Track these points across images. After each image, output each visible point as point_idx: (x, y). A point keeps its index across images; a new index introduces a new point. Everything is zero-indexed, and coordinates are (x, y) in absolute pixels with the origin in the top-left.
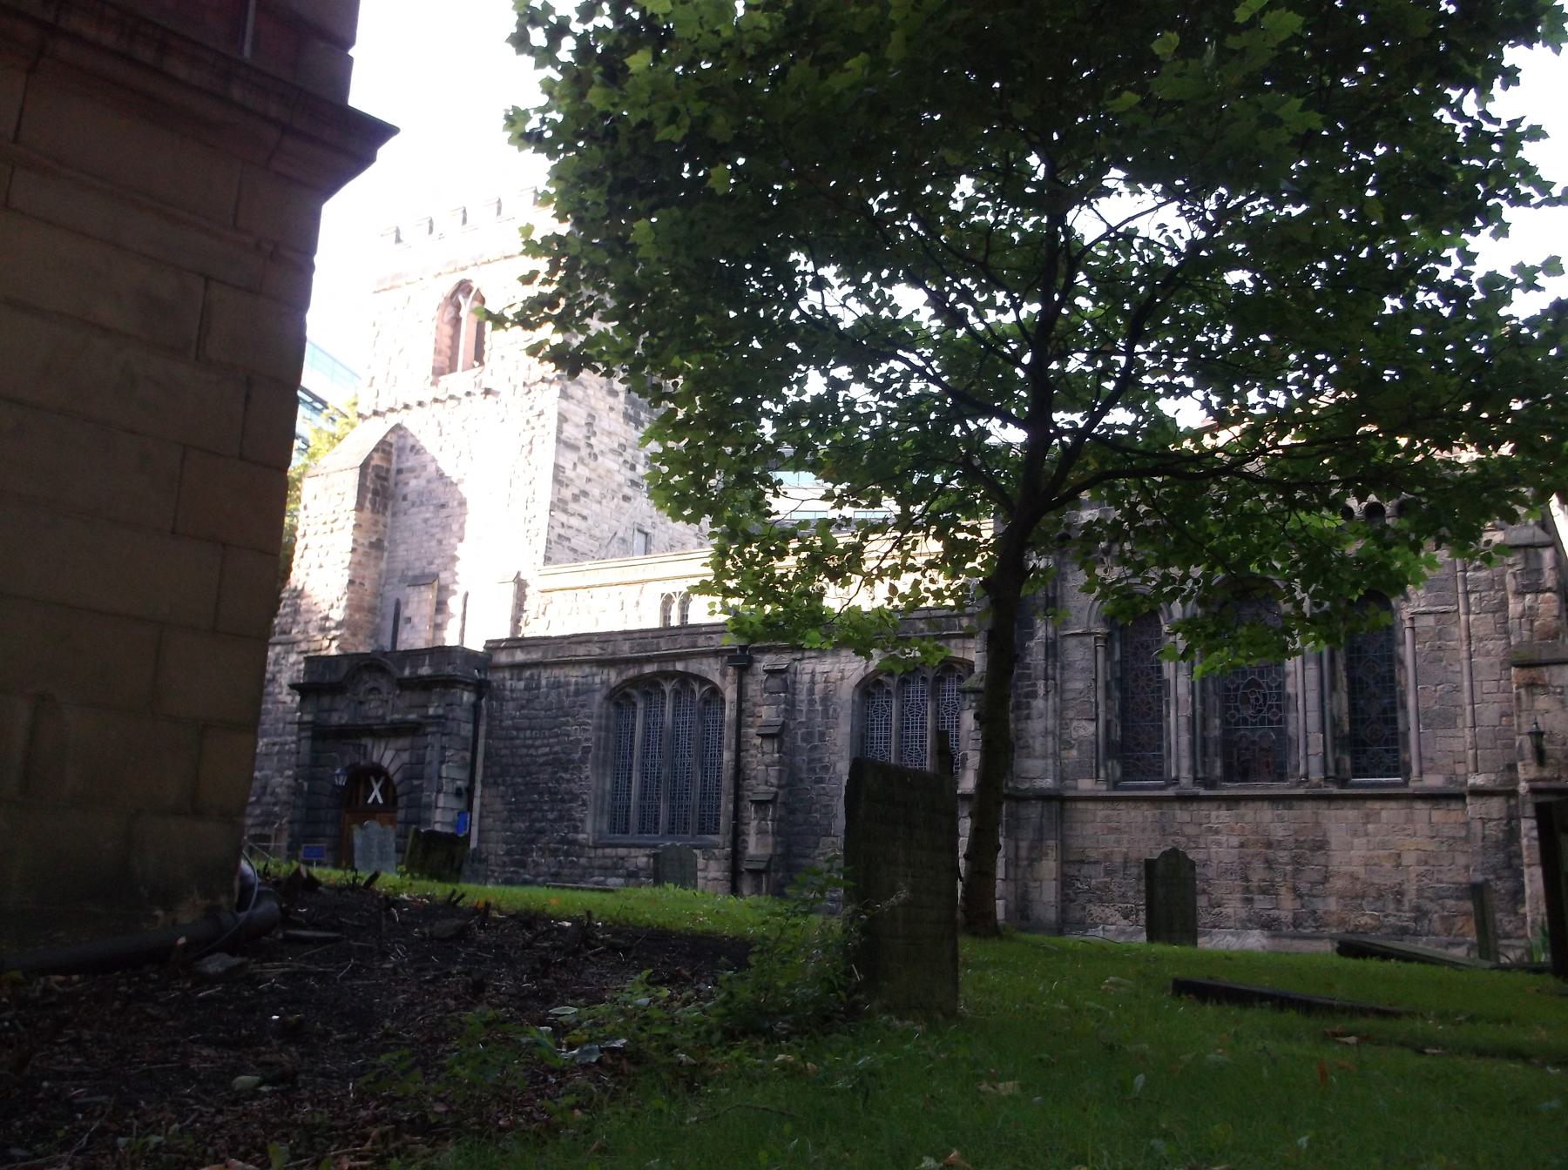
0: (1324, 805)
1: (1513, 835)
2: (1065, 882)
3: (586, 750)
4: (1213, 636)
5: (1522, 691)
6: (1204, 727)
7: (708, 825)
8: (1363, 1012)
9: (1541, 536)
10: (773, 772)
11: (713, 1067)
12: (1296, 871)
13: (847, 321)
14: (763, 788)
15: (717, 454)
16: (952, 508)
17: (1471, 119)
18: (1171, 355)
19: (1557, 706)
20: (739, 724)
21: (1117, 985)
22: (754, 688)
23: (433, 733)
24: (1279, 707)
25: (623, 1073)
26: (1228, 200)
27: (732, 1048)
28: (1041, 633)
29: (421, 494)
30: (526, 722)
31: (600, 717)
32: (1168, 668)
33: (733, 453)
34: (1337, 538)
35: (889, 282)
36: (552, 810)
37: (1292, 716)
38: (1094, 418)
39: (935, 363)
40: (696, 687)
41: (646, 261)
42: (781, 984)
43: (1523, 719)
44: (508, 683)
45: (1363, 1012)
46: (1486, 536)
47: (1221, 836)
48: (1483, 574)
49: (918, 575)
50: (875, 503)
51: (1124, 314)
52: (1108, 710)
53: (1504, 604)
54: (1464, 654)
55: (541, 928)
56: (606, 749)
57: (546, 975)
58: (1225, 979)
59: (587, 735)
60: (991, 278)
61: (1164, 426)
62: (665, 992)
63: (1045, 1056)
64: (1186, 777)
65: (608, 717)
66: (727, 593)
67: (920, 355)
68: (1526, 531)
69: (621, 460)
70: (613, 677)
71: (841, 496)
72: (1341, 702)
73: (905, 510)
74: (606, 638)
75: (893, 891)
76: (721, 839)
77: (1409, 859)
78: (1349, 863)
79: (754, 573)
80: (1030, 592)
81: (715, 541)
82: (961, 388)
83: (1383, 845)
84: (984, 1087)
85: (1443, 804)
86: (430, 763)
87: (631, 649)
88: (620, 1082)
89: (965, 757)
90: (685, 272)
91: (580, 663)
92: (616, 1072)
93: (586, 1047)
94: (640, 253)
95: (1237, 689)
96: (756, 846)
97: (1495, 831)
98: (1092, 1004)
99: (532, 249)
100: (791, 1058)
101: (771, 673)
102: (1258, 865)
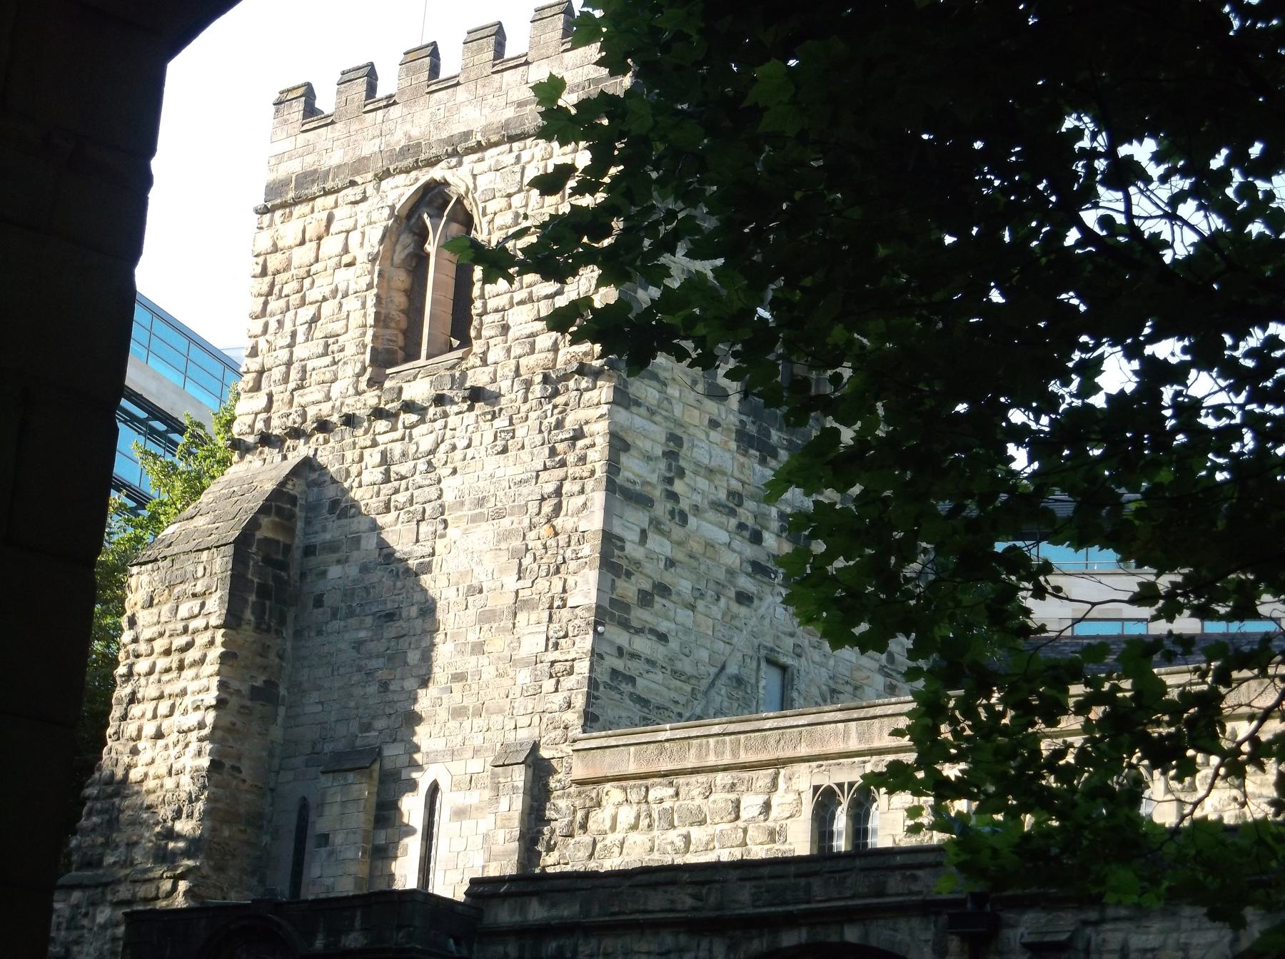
29: (348, 594)
69: (733, 522)
71: (1171, 595)
79: (998, 750)
81: (920, 684)
91: (656, 926)
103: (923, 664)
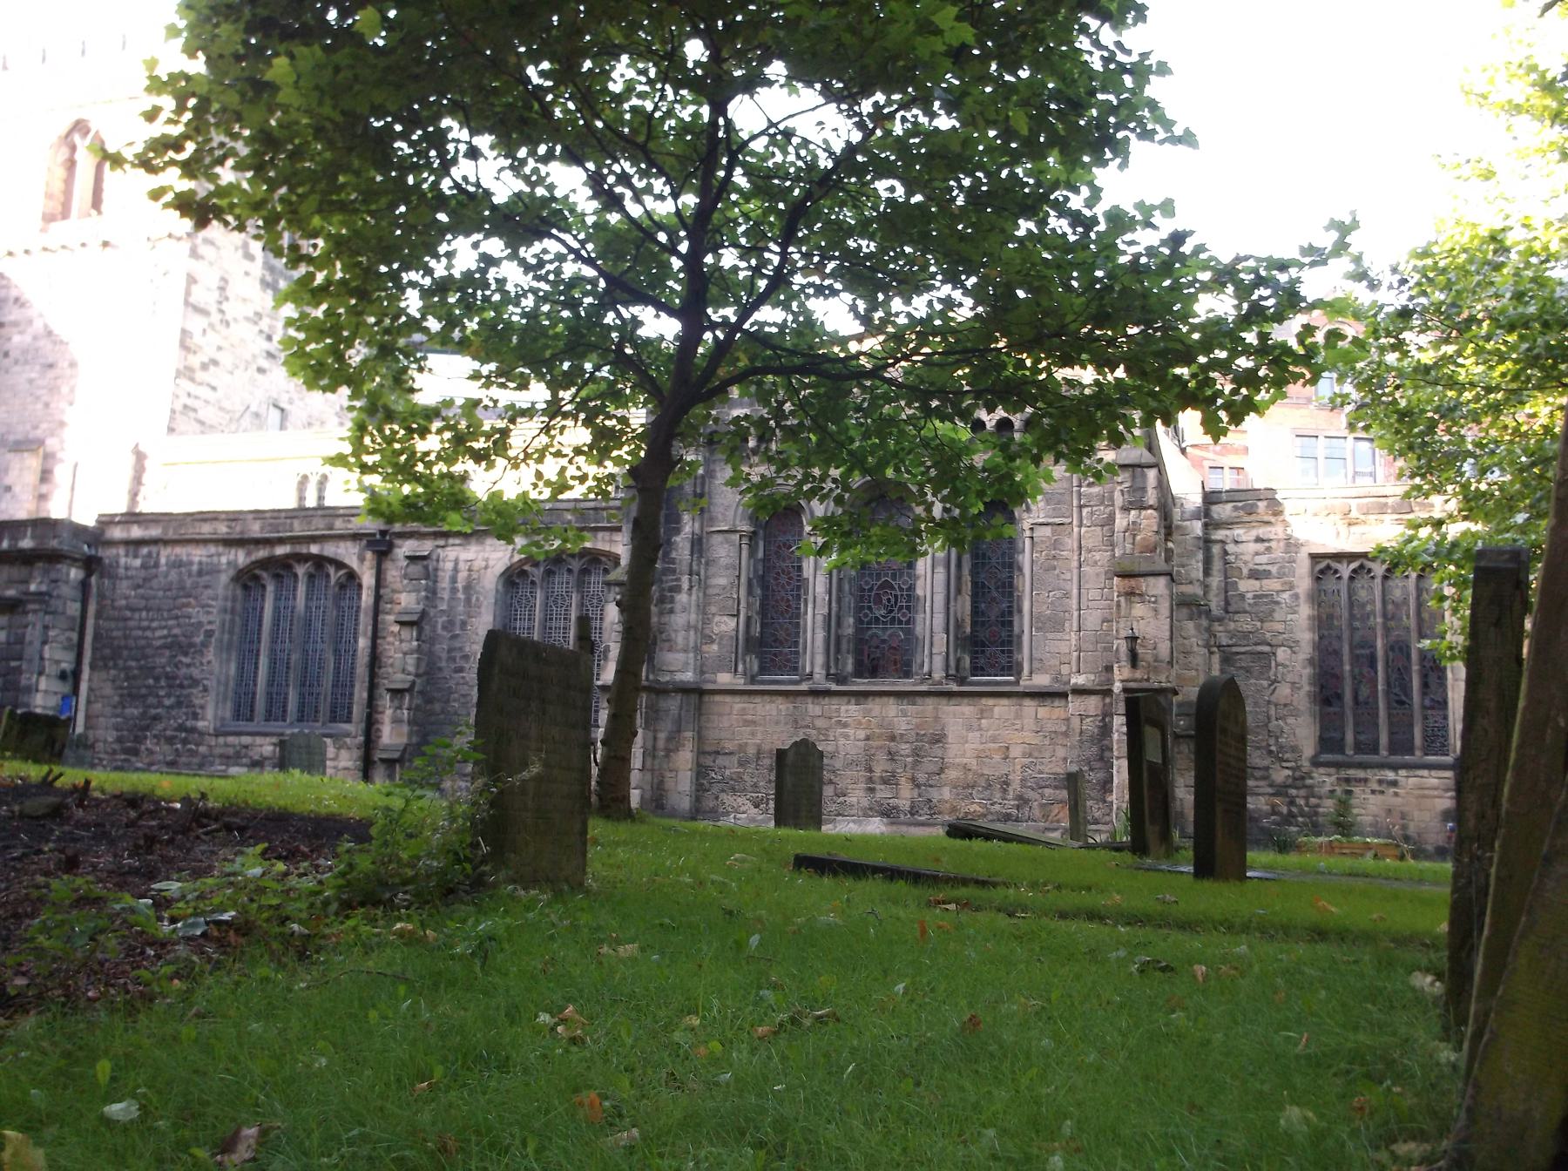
0: (944, 701)
1: (1106, 730)
2: (701, 772)
3: (209, 634)
4: (848, 534)
5: (1122, 599)
6: (839, 625)
7: (340, 713)
8: (964, 882)
9: (1144, 456)
10: (411, 661)
11: (324, 937)
12: (916, 763)
13: (500, 198)
14: (400, 676)
15: (358, 325)
16: (601, 396)
17: (1106, 48)
18: (823, 257)
19: (1152, 613)
20: (376, 611)
21: (743, 861)
22: (393, 574)
23: (35, 611)
24: (908, 608)
25: (229, 945)
26: (884, 107)
27: (348, 917)
28: (687, 529)
29: (25, 352)
30: (143, 603)
31: (226, 599)
32: (808, 566)
33: (376, 324)
34: (967, 449)
35: (546, 159)
36: (168, 696)
37: (919, 617)
38: (745, 313)
39: (590, 246)
40: (332, 570)
41: (286, 109)
42: (404, 856)
43: (1122, 625)
44: (123, 561)
45: (964, 882)
46: (1100, 455)
47: (848, 729)
48: (1096, 490)
49: (564, 462)
50: (523, 385)
51: (779, 213)
52: (749, 606)
53: (1111, 519)
54: (1075, 564)
55: (146, 806)
56: (231, 632)
57: (150, 851)
58: (843, 856)
59: (211, 618)
60: (651, 164)
61: (808, 325)
62: (281, 867)
63: (667, 921)
64: (819, 673)
65: (234, 599)
66: (365, 469)
67: (575, 237)
68: (1132, 453)
69: (257, 329)
70: (241, 557)
71: (488, 377)
72: (964, 605)
73: (555, 395)
74: (234, 517)
75: (525, 765)
76: (354, 728)
77: (1016, 752)
78: (963, 756)
79: (394, 451)
80: (676, 484)
81: (355, 414)
82: (616, 274)
83: (994, 740)
84: (605, 949)
85: (1048, 702)
86: (31, 643)
87: (262, 529)
88: (224, 953)
89: (607, 649)
90: (328, 125)
91: (205, 542)
92: (222, 944)
93: (191, 921)
94: (281, 97)
95: (871, 590)
96: (391, 735)
97: (1090, 726)
98: (714, 877)
99: (156, 86)
100: (410, 927)
101: (412, 559)
102: (882, 756)
103: (358, 404)
